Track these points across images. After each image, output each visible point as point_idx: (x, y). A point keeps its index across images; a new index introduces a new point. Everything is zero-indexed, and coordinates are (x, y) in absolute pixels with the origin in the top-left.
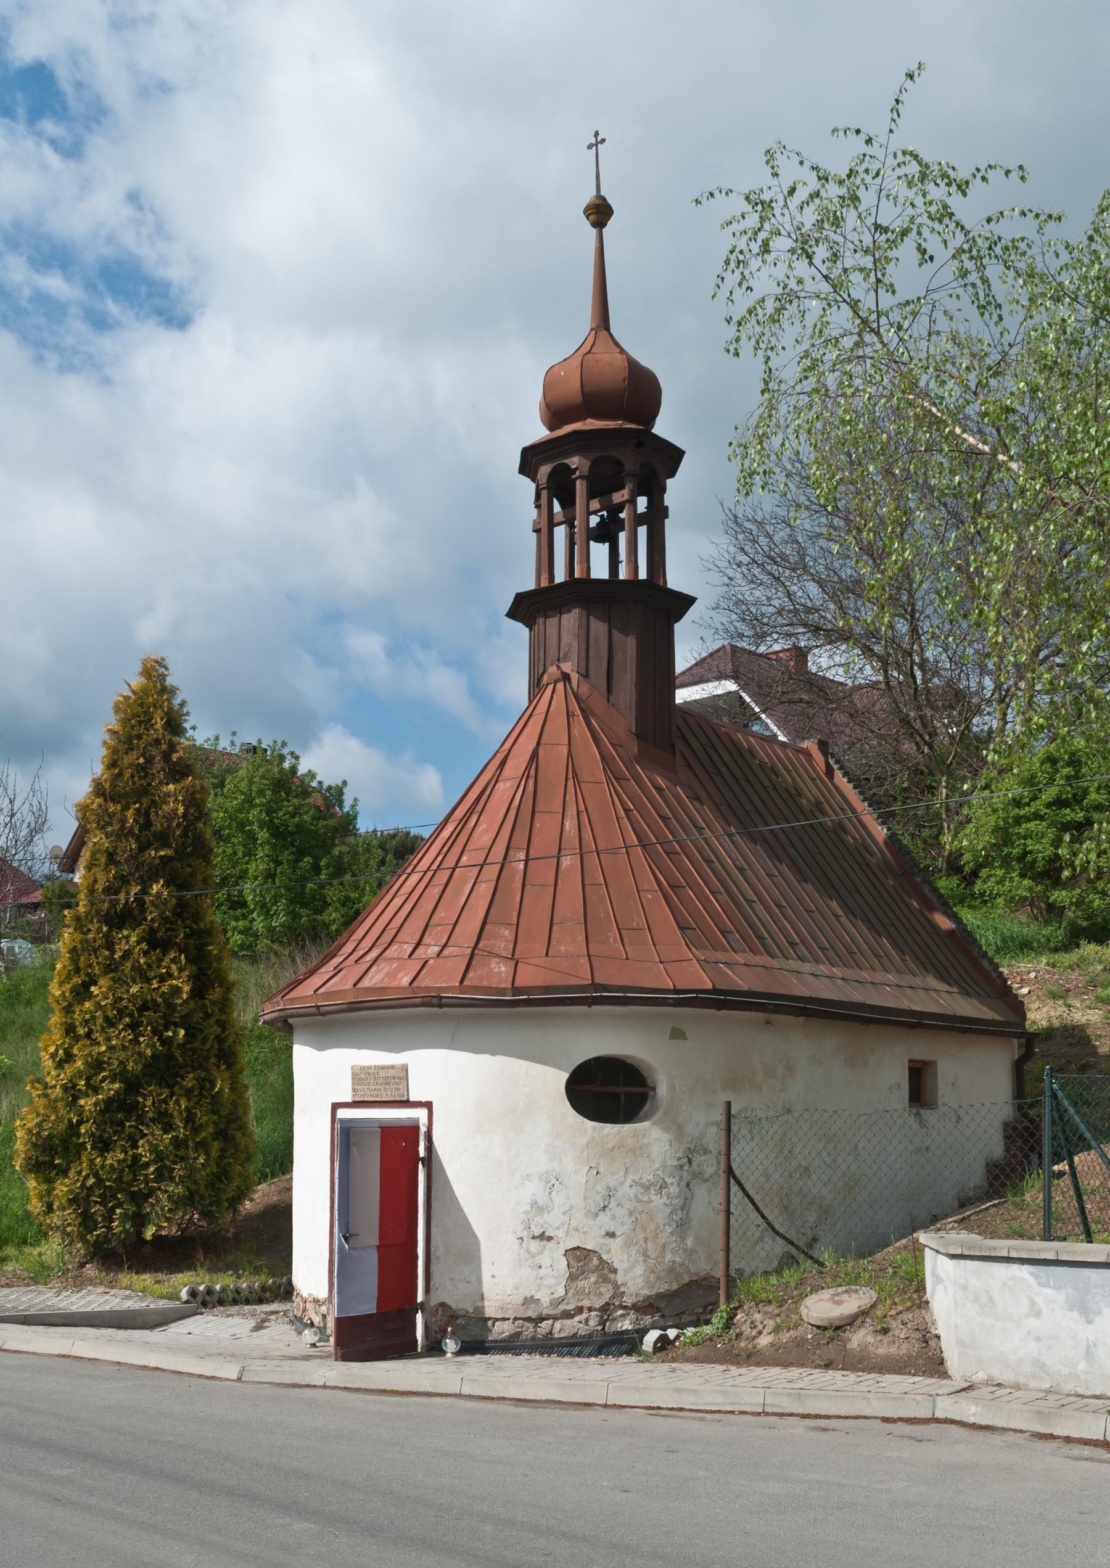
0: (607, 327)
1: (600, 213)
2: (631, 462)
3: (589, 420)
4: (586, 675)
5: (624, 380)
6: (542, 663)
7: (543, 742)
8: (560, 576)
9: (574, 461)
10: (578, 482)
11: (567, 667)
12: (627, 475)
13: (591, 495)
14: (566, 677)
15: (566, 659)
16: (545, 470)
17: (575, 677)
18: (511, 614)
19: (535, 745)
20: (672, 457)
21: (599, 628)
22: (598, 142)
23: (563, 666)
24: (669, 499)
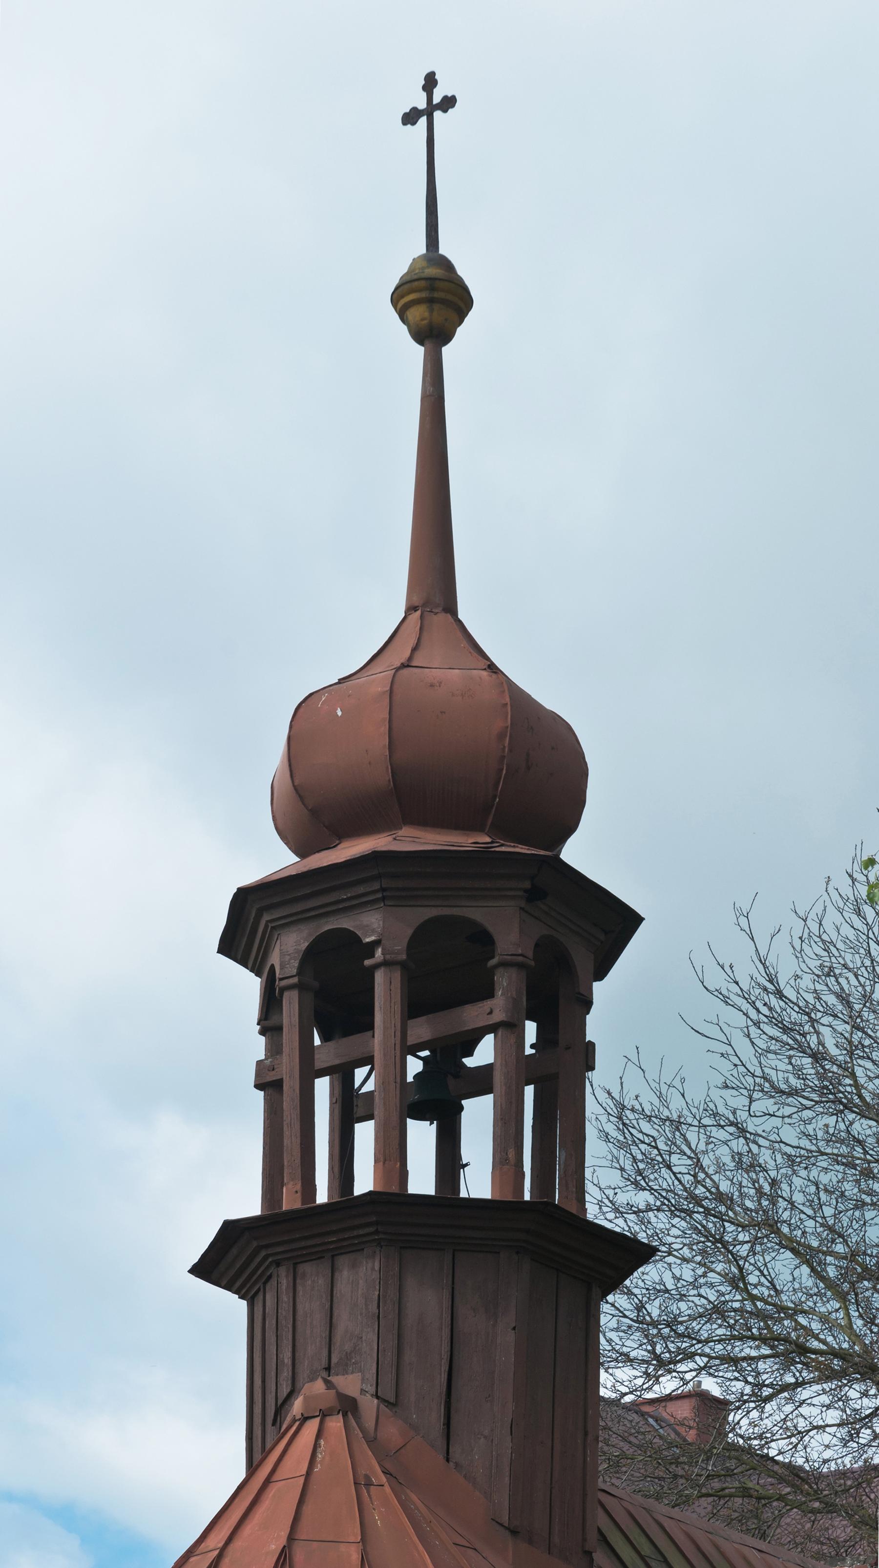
0: (451, 608)
1: (434, 302)
2: (511, 933)
3: (406, 831)
4: (392, 1403)
5: (501, 736)
6: (286, 1373)
7: (303, 1532)
8: (322, 1197)
9: (369, 924)
10: (379, 977)
11: (350, 1384)
12: (504, 964)
13: (415, 1007)
14: (348, 1407)
15: (345, 1366)
16: (289, 947)
17: (369, 1405)
18: (205, 1269)
19: (283, 1542)
20: (611, 924)
21: (425, 1301)
22: (431, 106)
23: (338, 1380)
24: (596, 1027)
